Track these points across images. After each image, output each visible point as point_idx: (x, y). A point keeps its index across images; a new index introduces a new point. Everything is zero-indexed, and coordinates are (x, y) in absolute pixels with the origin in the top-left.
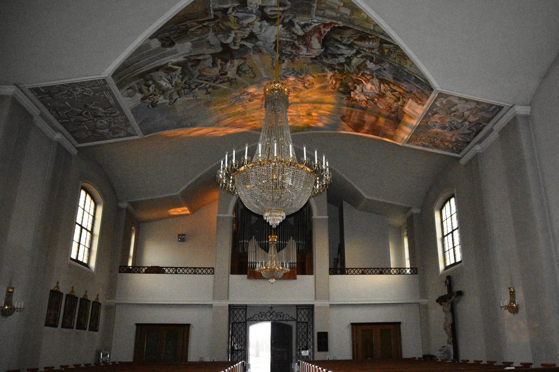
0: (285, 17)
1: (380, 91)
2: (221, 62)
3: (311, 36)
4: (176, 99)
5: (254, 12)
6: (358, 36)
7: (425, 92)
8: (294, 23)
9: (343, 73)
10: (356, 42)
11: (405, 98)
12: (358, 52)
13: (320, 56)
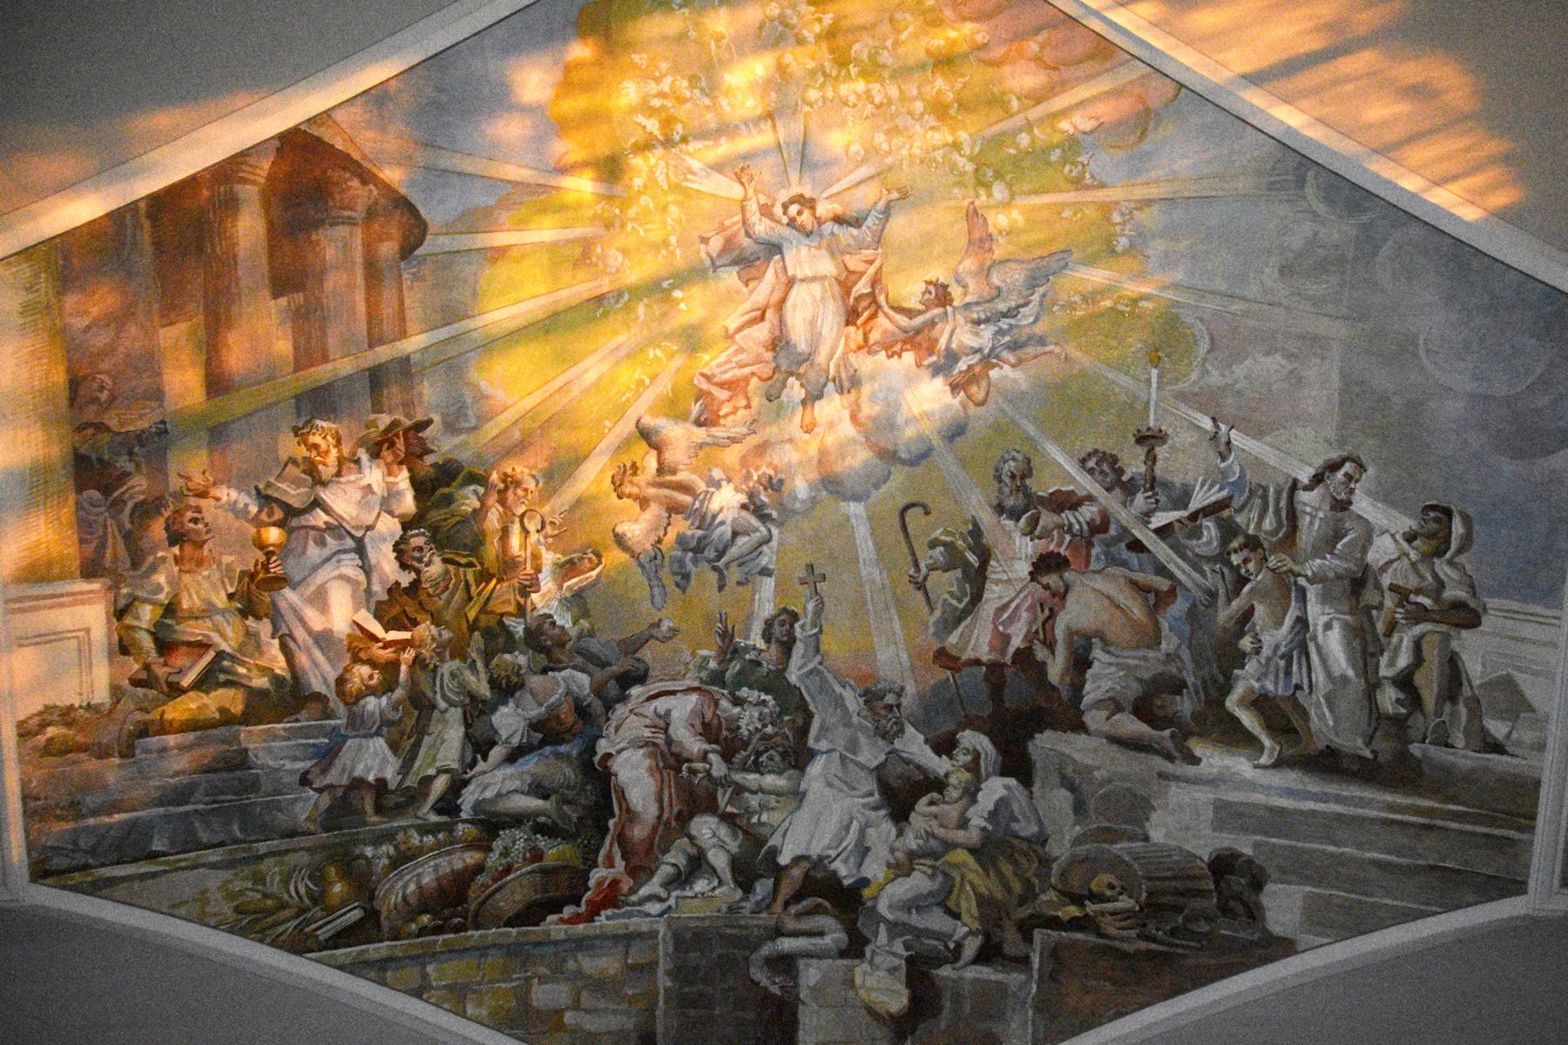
0: (768, 907)
1: (276, 617)
2: (1049, 661)
3: (660, 817)
4: (1318, 479)
5: (882, 927)
6: (471, 894)
7: (61, 818)
8: (736, 881)
9: (488, 634)
10: (471, 858)
11: (136, 683)
12: (449, 805)
13: (609, 707)
